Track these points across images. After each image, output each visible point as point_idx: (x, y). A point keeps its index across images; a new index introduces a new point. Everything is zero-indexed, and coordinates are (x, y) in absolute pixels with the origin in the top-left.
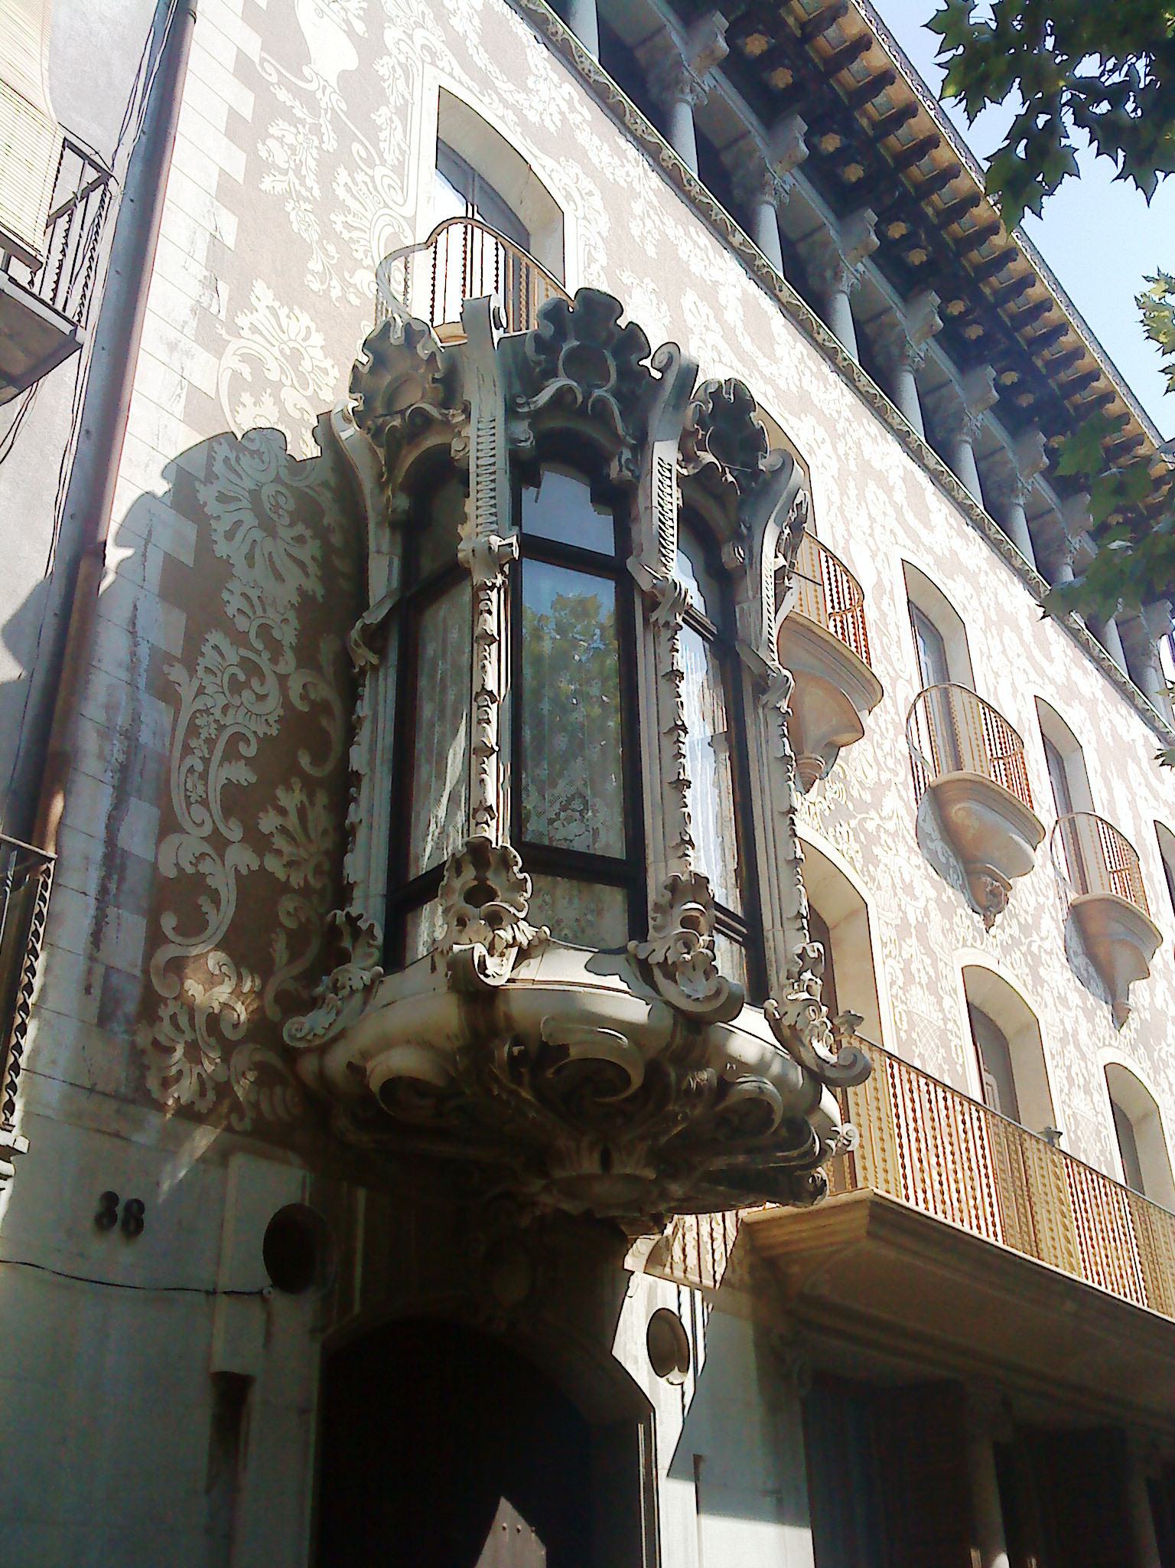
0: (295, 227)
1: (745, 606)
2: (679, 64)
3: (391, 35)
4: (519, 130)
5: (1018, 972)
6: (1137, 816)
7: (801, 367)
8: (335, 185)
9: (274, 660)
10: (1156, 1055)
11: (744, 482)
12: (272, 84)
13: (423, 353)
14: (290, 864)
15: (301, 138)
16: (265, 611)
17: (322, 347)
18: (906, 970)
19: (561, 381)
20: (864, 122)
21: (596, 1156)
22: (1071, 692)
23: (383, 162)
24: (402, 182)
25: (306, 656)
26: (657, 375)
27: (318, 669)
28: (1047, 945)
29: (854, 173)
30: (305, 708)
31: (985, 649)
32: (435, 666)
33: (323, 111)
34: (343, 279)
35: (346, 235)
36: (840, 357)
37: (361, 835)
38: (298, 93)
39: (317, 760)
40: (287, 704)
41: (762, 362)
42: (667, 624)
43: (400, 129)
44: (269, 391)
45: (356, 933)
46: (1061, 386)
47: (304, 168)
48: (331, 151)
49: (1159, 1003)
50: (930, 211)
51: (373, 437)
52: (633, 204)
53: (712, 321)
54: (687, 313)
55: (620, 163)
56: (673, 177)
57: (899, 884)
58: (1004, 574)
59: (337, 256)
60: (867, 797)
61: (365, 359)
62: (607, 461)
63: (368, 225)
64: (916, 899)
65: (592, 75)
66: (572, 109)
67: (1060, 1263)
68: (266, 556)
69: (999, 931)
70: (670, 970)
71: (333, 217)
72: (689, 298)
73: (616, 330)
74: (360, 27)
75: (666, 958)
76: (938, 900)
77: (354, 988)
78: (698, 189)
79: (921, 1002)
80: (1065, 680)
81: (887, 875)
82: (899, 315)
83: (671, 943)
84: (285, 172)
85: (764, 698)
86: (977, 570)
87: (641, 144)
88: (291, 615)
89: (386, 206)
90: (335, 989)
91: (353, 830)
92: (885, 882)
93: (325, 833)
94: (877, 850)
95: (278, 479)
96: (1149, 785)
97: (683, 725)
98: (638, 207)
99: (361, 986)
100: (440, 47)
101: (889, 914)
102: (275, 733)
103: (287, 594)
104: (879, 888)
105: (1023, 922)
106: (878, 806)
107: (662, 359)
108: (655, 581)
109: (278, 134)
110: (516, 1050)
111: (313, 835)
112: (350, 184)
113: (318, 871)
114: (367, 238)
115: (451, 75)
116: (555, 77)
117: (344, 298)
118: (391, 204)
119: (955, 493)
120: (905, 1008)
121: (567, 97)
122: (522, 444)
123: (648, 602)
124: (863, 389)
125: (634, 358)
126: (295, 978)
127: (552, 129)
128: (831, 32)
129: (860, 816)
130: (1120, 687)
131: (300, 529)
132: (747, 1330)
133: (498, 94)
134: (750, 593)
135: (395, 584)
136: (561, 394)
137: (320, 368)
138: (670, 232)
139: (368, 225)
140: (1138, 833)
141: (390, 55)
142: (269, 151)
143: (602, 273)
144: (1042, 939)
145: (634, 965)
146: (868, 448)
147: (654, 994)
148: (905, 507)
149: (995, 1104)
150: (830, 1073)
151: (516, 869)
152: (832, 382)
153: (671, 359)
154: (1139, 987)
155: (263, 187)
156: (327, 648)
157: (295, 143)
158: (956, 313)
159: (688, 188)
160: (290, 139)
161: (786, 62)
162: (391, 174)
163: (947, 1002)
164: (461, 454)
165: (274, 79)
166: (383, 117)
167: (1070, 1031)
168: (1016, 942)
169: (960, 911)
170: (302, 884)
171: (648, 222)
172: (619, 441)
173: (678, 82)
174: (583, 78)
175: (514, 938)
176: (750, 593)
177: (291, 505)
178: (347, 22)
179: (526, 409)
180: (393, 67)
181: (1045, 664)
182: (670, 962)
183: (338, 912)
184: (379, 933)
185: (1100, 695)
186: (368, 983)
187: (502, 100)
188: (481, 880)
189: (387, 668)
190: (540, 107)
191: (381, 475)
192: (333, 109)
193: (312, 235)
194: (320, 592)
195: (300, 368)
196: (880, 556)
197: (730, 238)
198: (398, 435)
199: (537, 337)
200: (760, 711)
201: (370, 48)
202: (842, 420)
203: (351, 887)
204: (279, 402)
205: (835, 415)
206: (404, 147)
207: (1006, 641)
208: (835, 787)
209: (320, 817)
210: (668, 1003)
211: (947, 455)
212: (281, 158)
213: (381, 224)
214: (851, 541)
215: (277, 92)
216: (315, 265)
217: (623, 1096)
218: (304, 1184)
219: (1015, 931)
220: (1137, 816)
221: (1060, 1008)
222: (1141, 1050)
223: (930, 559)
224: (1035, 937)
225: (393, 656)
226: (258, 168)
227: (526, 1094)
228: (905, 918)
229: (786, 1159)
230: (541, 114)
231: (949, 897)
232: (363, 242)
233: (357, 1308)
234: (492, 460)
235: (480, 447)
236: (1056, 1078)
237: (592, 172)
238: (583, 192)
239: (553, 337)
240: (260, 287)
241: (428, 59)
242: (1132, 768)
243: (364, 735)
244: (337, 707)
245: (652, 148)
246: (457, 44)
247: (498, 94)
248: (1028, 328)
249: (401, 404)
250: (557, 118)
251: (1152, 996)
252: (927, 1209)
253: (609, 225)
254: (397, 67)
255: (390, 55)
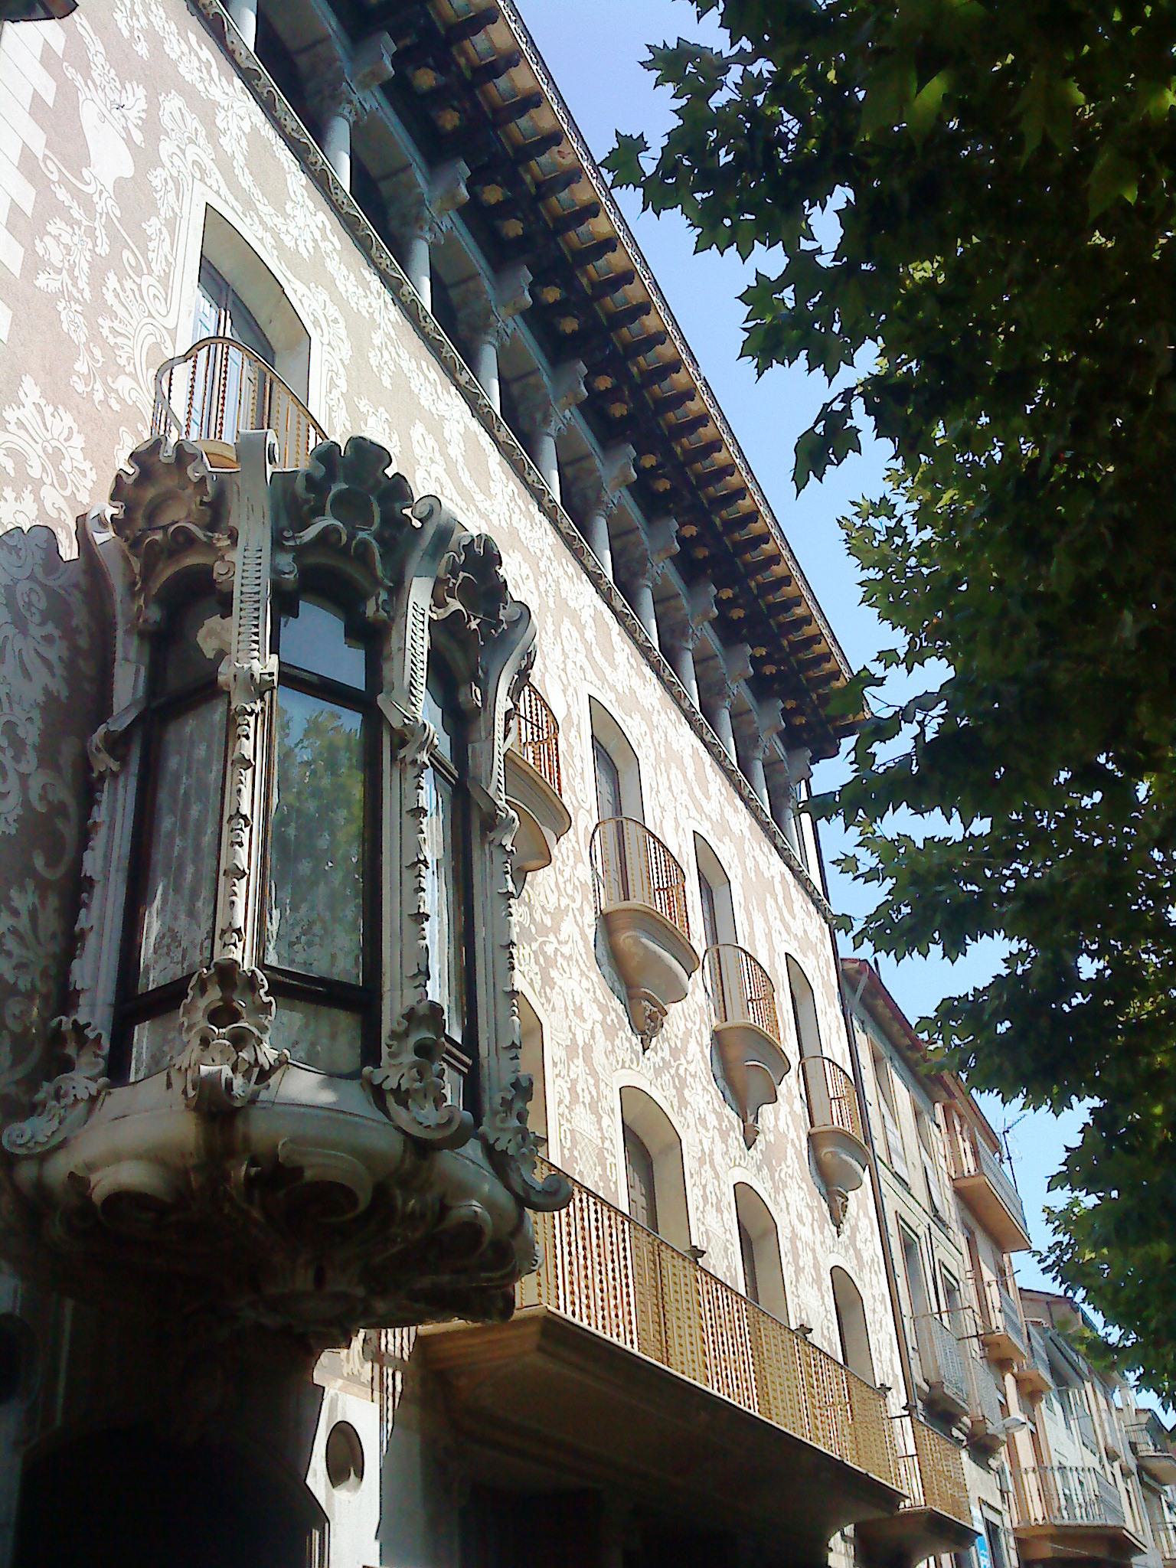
0: (65, 326)
1: (477, 745)
2: (421, 202)
3: (166, 148)
4: (275, 253)
5: (667, 1093)
6: (772, 949)
7: (512, 505)
8: (104, 290)
9: (17, 758)
10: (777, 1177)
11: (485, 630)
12: (54, 182)
13: (193, 474)
14: (21, 966)
15: (76, 239)
16: (11, 709)
17: (82, 449)
18: (572, 1090)
19: (327, 521)
20: (584, 281)
21: (311, 1273)
22: (723, 827)
23: (150, 272)
24: (167, 294)
25: (48, 757)
26: (417, 524)
27: (57, 768)
28: (692, 1068)
29: (570, 325)
30: (41, 808)
31: (654, 785)
32: (177, 779)
33: (98, 215)
34: (105, 383)
35: (111, 340)
36: (546, 499)
37: (91, 940)
38: (76, 194)
39: (51, 864)
40: (26, 803)
41: (479, 497)
42: (414, 762)
43: (168, 240)
44: (30, 487)
45: (82, 1041)
46: (735, 544)
47: (76, 269)
48: (103, 255)
49: (782, 1126)
50: (635, 370)
51: (131, 547)
52: (373, 335)
53: (437, 454)
54: (415, 444)
55: (363, 294)
56: (410, 310)
57: (571, 1007)
58: (674, 714)
59: (102, 360)
60: (548, 922)
61: (131, 471)
62: (364, 598)
63: (132, 332)
64: (584, 1020)
65: (344, 207)
66: (325, 238)
67: (697, 1377)
68: (17, 651)
69: (653, 1053)
70: (403, 1097)
71: (100, 320)
72: (418, 431)
73: (383, 479)
74: (138, 137)
75: (399, 1084)
76: (603, 1023)
77: (79, 1097)
78: (432, 327)
79: (583, 1120)
80: (719, 817)
81: (560, 997)
82: (597, 462)
83: (404, 1070)
84: (59, 272)
85: (491, 836)
86: (651, 709)
87: (385, 278)
88: (36, 714)
89: (150, 315)
90: (58, 1096)
91: (83, 934)
92: (559, 1003)
93: (53, 936)
94: (554, 973)
95: (31, 577)
96: (783, 920)
97: (425, 860)
98: (377, 339)
99: (86, 1097)
100: (210, 165)
101: (560, 1035)
102: (13, 832)
103: (33, 692)
104: (554, 1009)
105: (673, 1046)
106: (556, 930)
107: (422, 509)
108: (406, 721)
109: (55, 232)
110: (253, 1170)
111: (42, 935)
112: (119, 290)
113: (44, 974)
114: (131, 345)
115: (218, 193)
116: (311, 205)
117: (105, 402)
118: (154, 314)
119: (637, 635)
120: (569, 1126)
121: (320, 226)
122: (287, 576)
123: (396, 740)
124: (564, 531)
125: (397, 506)
126: (18, 1083)
127: (305, 255)
128: (564, 195)
129: (541, 939)
130: (764, 826)
131: (50, 628)
132: (416, 1440)
133: (259, 216)
134: (483, 734)
135: (141, 691)
136: (326, 533)
137: (79, 470)
138: (405, 365)
139: (132, 332)
140: (772, 965)
141: (163, 166)
142: (46, 249)
143: (341, 399)
144: (688, 1062)
145: (368, 1090)
146: (565, 585)
147: (386, 1120)
148: (594, 645)
149: (642, 1219)
150: (534, 1198)
151: (262, 992)
152: (537, 521)
153: (431, 512)
154: (766, 1110)
155: (37, 283)
156: (68, 750)
157: (71, 244)
158: (648, 466)
159: (423, 324)
160: (66, 239)
161: (519, 215)
162: (157, 284)
163: (606, 1120)
164: (224, 577)
165: (55, 177)
166: (153, 228)
167: (707, 1151)
168: (666, 1065)
169: (621, 1034)
170: (29, 986)
171: (385, 353)
172: (378, 583)
173: (418, 218)
174: (336, 208)
175: (256, 1059)
176: (483, 734)
177: (43, 604)
178: (126, 129)
179: (291, 543)
180: (165, 180)
181: (704, 802)
182: (403, 1089)
183: (64, 1018)
184: (106, 1042)
185: (747, 834)
186: (94, 1093)
187: (262, 222)
188: (227, 1001)
189: (126, 779)
190: (295, 232)
191: (134, 584)
192: (107, 213)
193: (80, 337)
194: (65, 693)
195: (61, 468)
196: (571, 690)
197: (458, 376)
198: (157, 548)
199: (308, 477)
200: (487, 847)
201: (146, 158)
202: (545, 558)
203: (78, 993)
204: (38, 500)
205: (539, 553)
206: (171, 260)
207: (672, 777)
208: (520, 910)
209: (50, 922)
210: (399, 1129)
211: (632, 598)
212: (56, 256)
213: (144, 332)
214: (547, 675)
215: (57, 190)
216: (81, 367)
217: (351, 1215)
218: (15, 1292)
219: (666, 1054)
220: (772, 949)
221: (700, 1128)
222: (765, 1171)
223: (612, 696)
224: (683, 1061)
225: (134, 766)
226: (35, 264)
227: (256, 1214)
228: (574, 1040)
229: (489, 1280)
230: (296, 240)
231: (612, 1021)
232: (127, 349)
233: (59, 1422)
234: (257, 589)
235: (245, 574)
236: (694, 1195)
237: (339, 301)
238: (330, 319)
239: (323, 478)
240: (28, 382)
241: (198, 175)
242: (770, 901)
243: (99, 841)
244: (73, 811)
245: (394, 282)
246: (225, 164)
247: (259, 216)
248: (711, 489)
249: (164, 520)
250: (310, 244)
251: (777, 1119)
252: (590, 1324)
253: (350, 353)
254: (169, 180)
255: (163, 166)
